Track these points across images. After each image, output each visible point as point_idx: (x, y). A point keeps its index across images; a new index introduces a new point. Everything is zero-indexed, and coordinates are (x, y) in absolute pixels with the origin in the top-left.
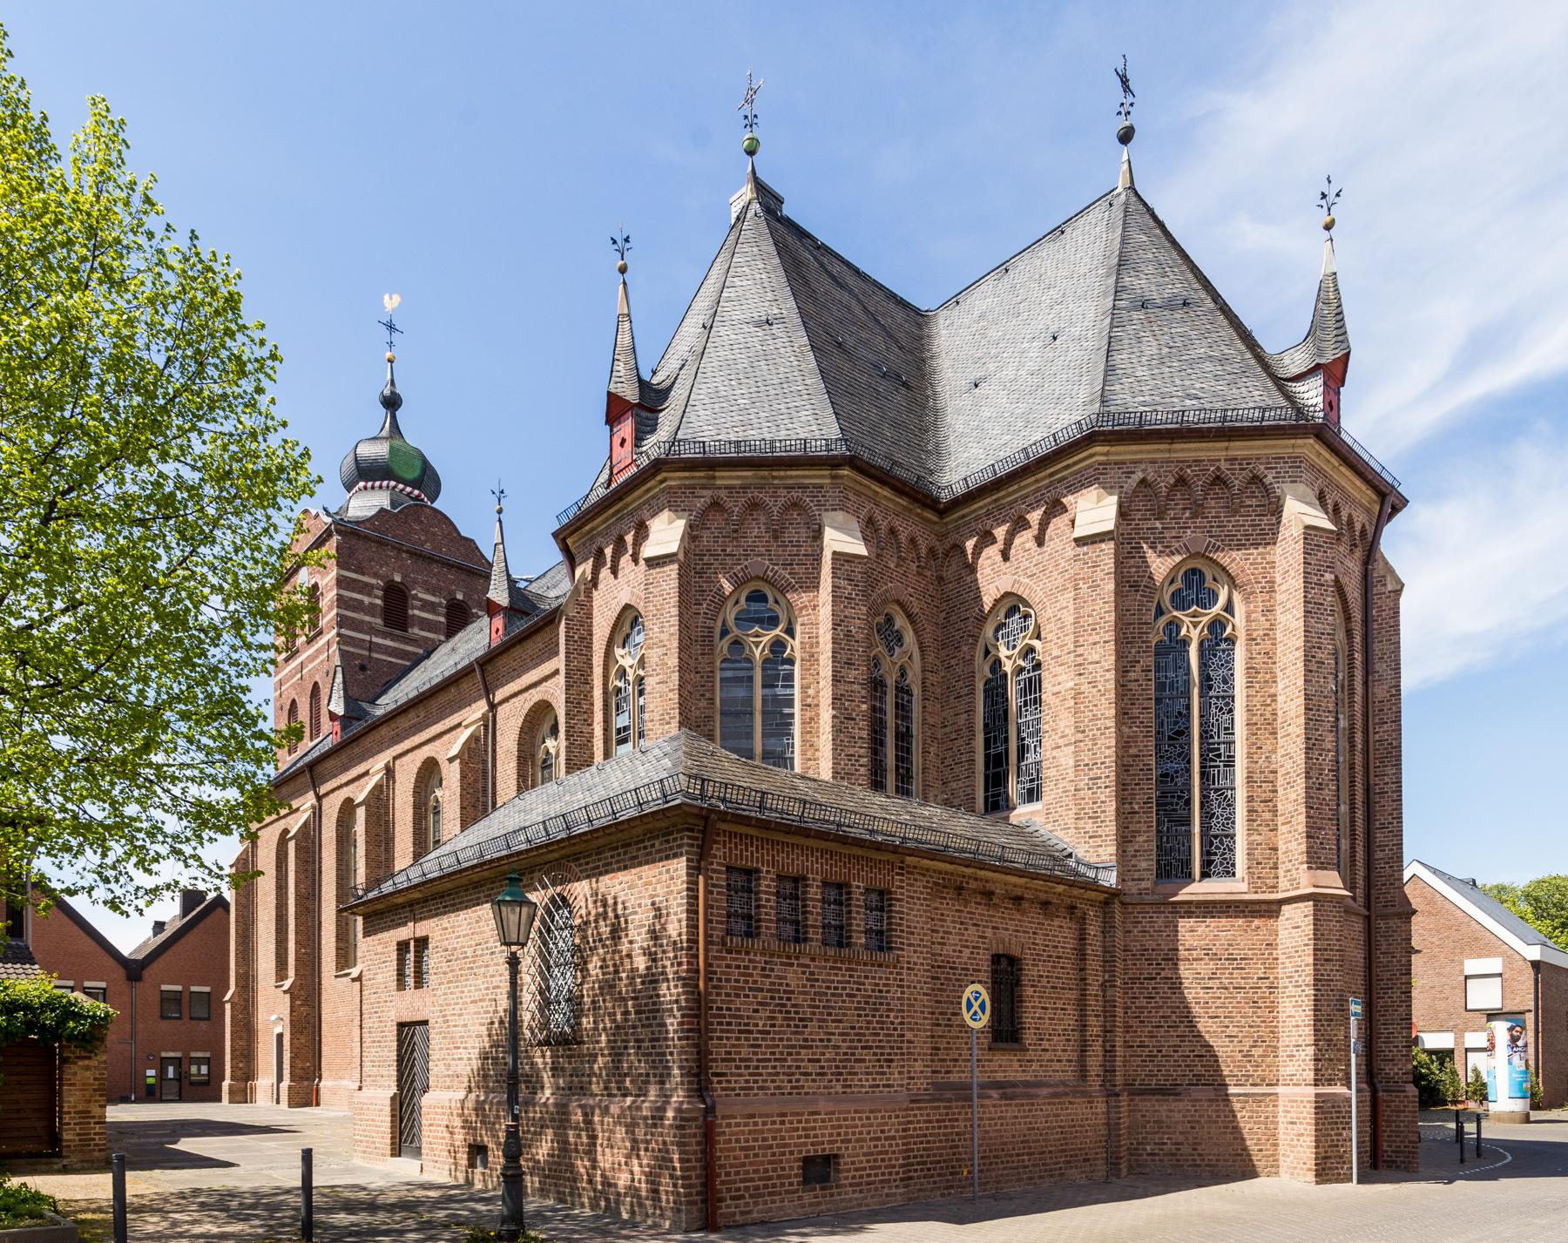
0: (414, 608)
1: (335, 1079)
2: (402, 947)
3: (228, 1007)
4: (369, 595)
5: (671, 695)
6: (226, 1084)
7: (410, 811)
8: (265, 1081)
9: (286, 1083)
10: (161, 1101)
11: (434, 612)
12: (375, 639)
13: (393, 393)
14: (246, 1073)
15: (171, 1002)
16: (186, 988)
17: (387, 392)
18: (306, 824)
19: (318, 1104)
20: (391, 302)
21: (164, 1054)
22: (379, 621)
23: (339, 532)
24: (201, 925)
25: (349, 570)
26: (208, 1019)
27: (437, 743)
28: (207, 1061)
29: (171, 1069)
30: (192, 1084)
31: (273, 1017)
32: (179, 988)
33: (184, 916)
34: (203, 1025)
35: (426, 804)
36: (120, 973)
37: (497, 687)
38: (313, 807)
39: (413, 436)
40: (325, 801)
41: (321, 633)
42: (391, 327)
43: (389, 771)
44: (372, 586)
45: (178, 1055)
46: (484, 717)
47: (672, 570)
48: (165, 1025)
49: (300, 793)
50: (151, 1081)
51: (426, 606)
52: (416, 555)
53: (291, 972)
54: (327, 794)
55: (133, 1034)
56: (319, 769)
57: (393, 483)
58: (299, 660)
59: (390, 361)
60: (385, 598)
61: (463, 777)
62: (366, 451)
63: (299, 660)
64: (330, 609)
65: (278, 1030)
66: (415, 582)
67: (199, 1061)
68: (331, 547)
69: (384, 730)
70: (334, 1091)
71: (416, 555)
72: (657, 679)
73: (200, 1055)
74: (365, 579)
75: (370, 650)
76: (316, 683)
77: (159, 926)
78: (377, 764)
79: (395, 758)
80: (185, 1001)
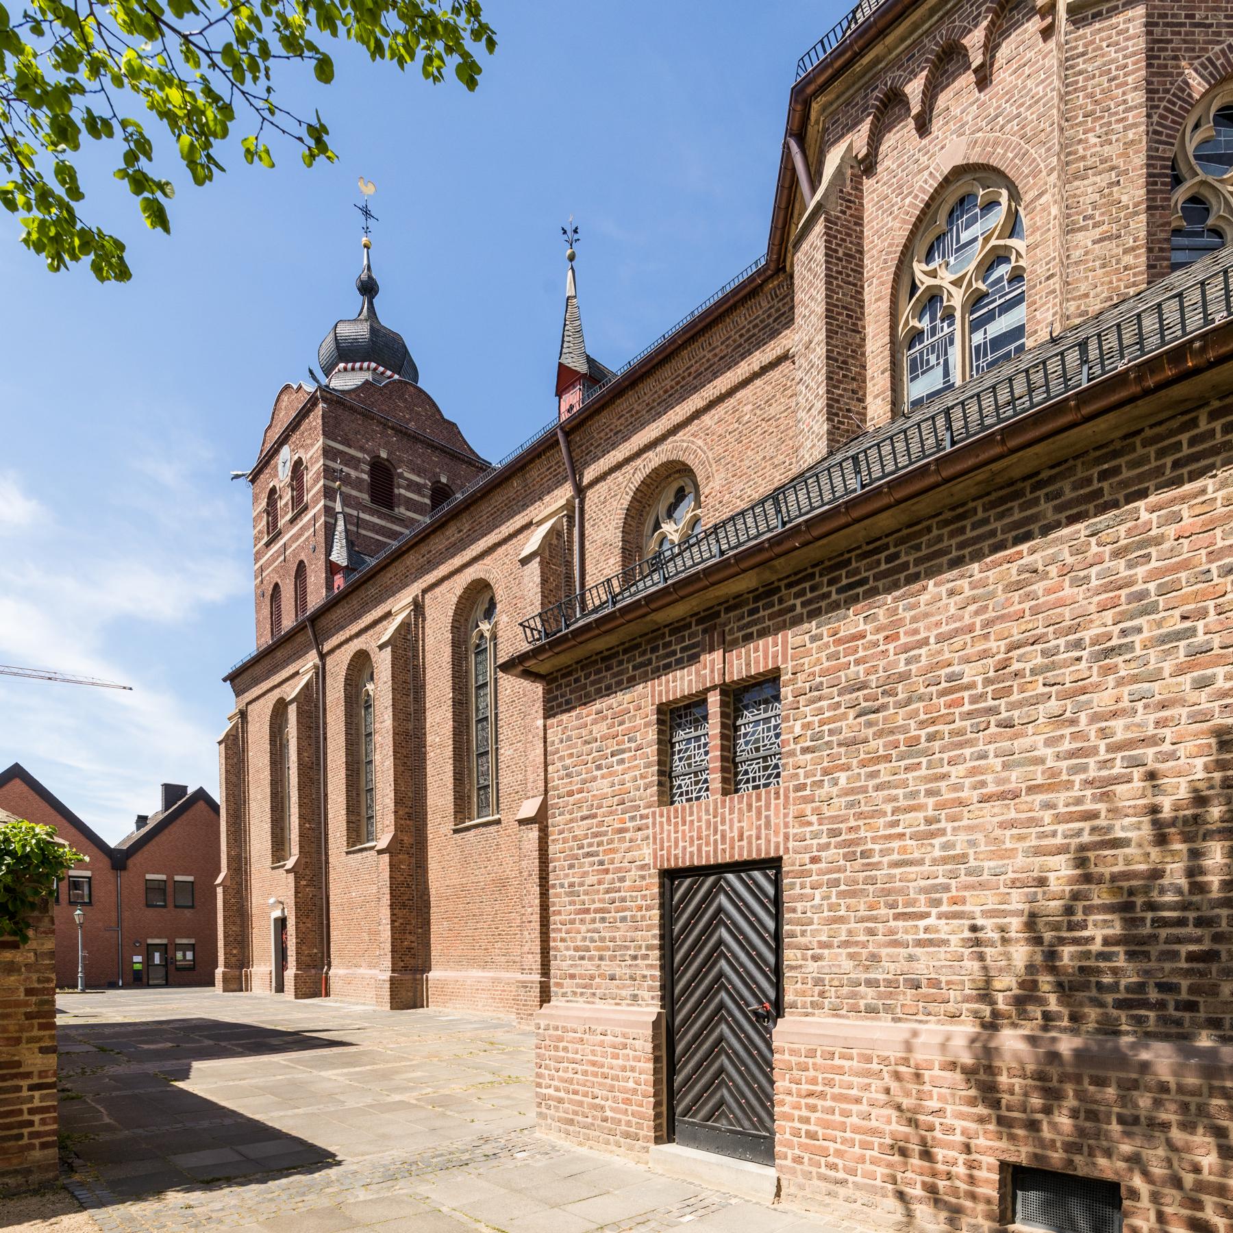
0: (399, 487)
1: (348, 967)
2: (676, 716)
3: (220, 890)
4: (356, 469)
5: (1129, 259)
6: (219, 971)
7: (447, 652)
8: (262, 968)
9: (290, 973)
10: (149, 986)
11: (419, 493)
12: (362, 515)
13: (370, 277)
14: (241, 961)
15: (155, 892)
16: (170, 877)
17: (364, 277)
18: (307, 685)
19: (327, 995)
20: (369, 190)
21: (150, 941)
22: (366, 496)
23: (325, 400)
24: (184, 817)
25: (335, 440)
26: (192, 907)
27: (487, 560)
28: (192, 947)
29: (157, 955)
30: (178, 969)
31: (272, 901)
32: (164, 877)
33: (166, 810)
34: (188, 913)
35: (466, 642)
36: (105, 862)
37: (587, 464)
38: (316, 667)
39: (387, 320)
40: (329, 661)
41: (306, 508)
42: (366, 213)
43: (418, 607)
44: (359, 460)
45: (164, 941)
46: (569, 505)
47: (535, 564)
48: (150, 913)
49: (299, 654)
50: (138, 967)
51: (412, 486)
52: (401, 432)
53: (295, 850)
54: (332, 651)
55: (119, 921)
56: (323, 622)
57: (373, 365)
58: (281, 542)
59: (366, 246)
60: (372, 474)
61: (544, 581)
62: (346, 330)
63: (281, 542)
64: (316, 481)
65: (277, 913)
66: (401, 461)
67: (184, 948)
68: (315, 419)
69: (411, 559)
70: (348, 981)
71: (401, 432)
72: (1096, 233)
73: (185, 941)
74: (352, 452)
75: (358, 526)
76: (301, 562)
77: (142, 820)
78: (401, 604)
79: (425, 592)
80: (170, 890)
